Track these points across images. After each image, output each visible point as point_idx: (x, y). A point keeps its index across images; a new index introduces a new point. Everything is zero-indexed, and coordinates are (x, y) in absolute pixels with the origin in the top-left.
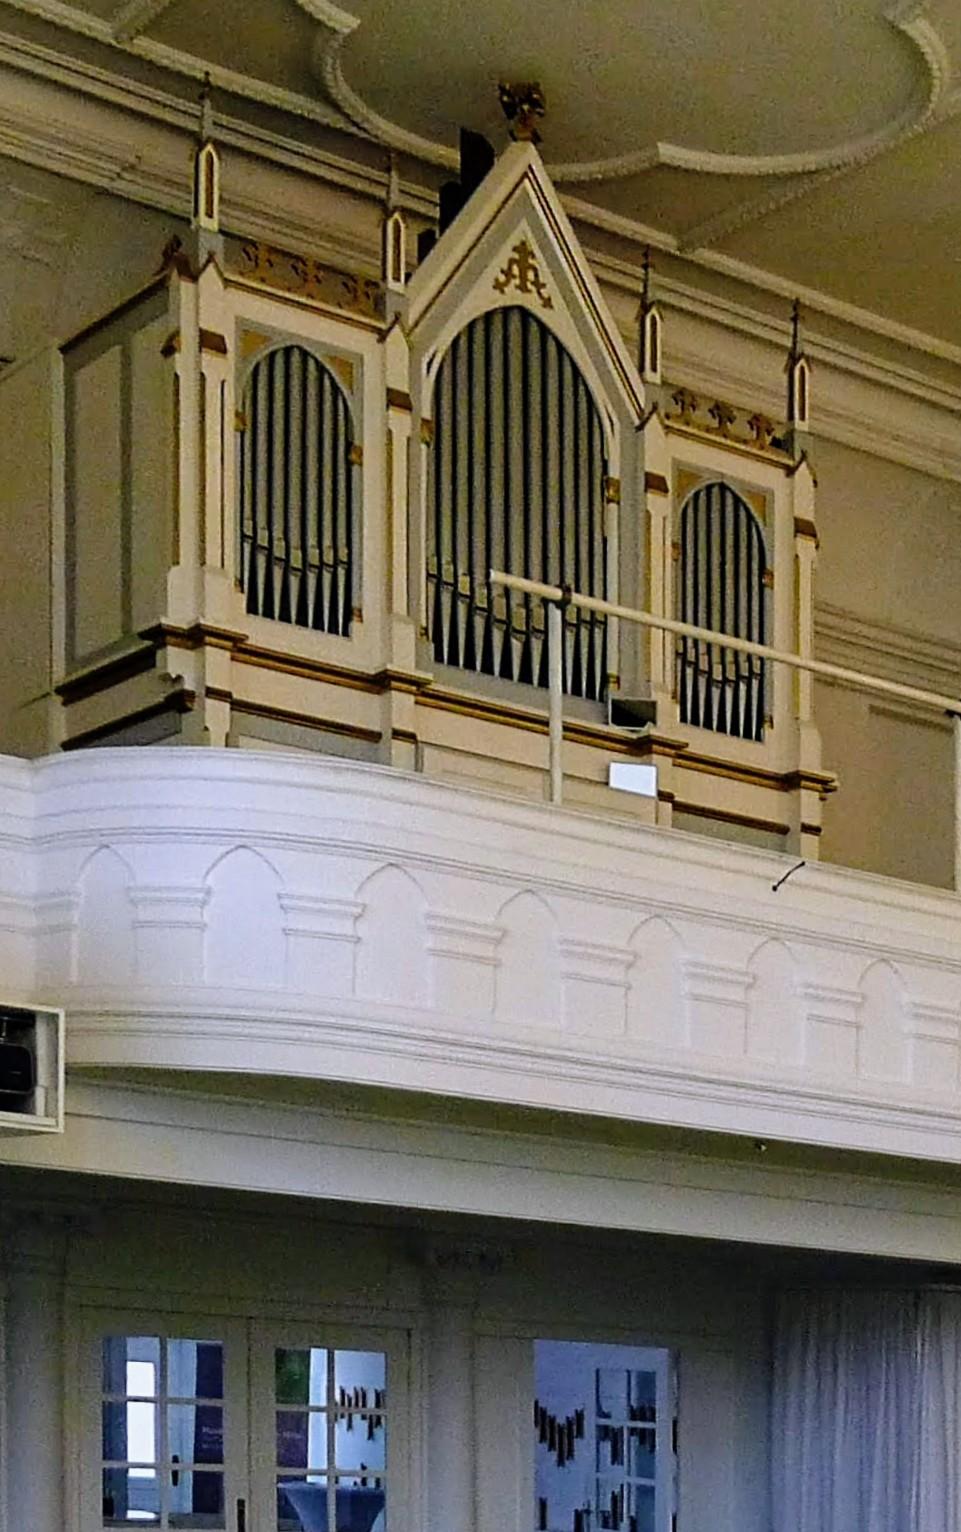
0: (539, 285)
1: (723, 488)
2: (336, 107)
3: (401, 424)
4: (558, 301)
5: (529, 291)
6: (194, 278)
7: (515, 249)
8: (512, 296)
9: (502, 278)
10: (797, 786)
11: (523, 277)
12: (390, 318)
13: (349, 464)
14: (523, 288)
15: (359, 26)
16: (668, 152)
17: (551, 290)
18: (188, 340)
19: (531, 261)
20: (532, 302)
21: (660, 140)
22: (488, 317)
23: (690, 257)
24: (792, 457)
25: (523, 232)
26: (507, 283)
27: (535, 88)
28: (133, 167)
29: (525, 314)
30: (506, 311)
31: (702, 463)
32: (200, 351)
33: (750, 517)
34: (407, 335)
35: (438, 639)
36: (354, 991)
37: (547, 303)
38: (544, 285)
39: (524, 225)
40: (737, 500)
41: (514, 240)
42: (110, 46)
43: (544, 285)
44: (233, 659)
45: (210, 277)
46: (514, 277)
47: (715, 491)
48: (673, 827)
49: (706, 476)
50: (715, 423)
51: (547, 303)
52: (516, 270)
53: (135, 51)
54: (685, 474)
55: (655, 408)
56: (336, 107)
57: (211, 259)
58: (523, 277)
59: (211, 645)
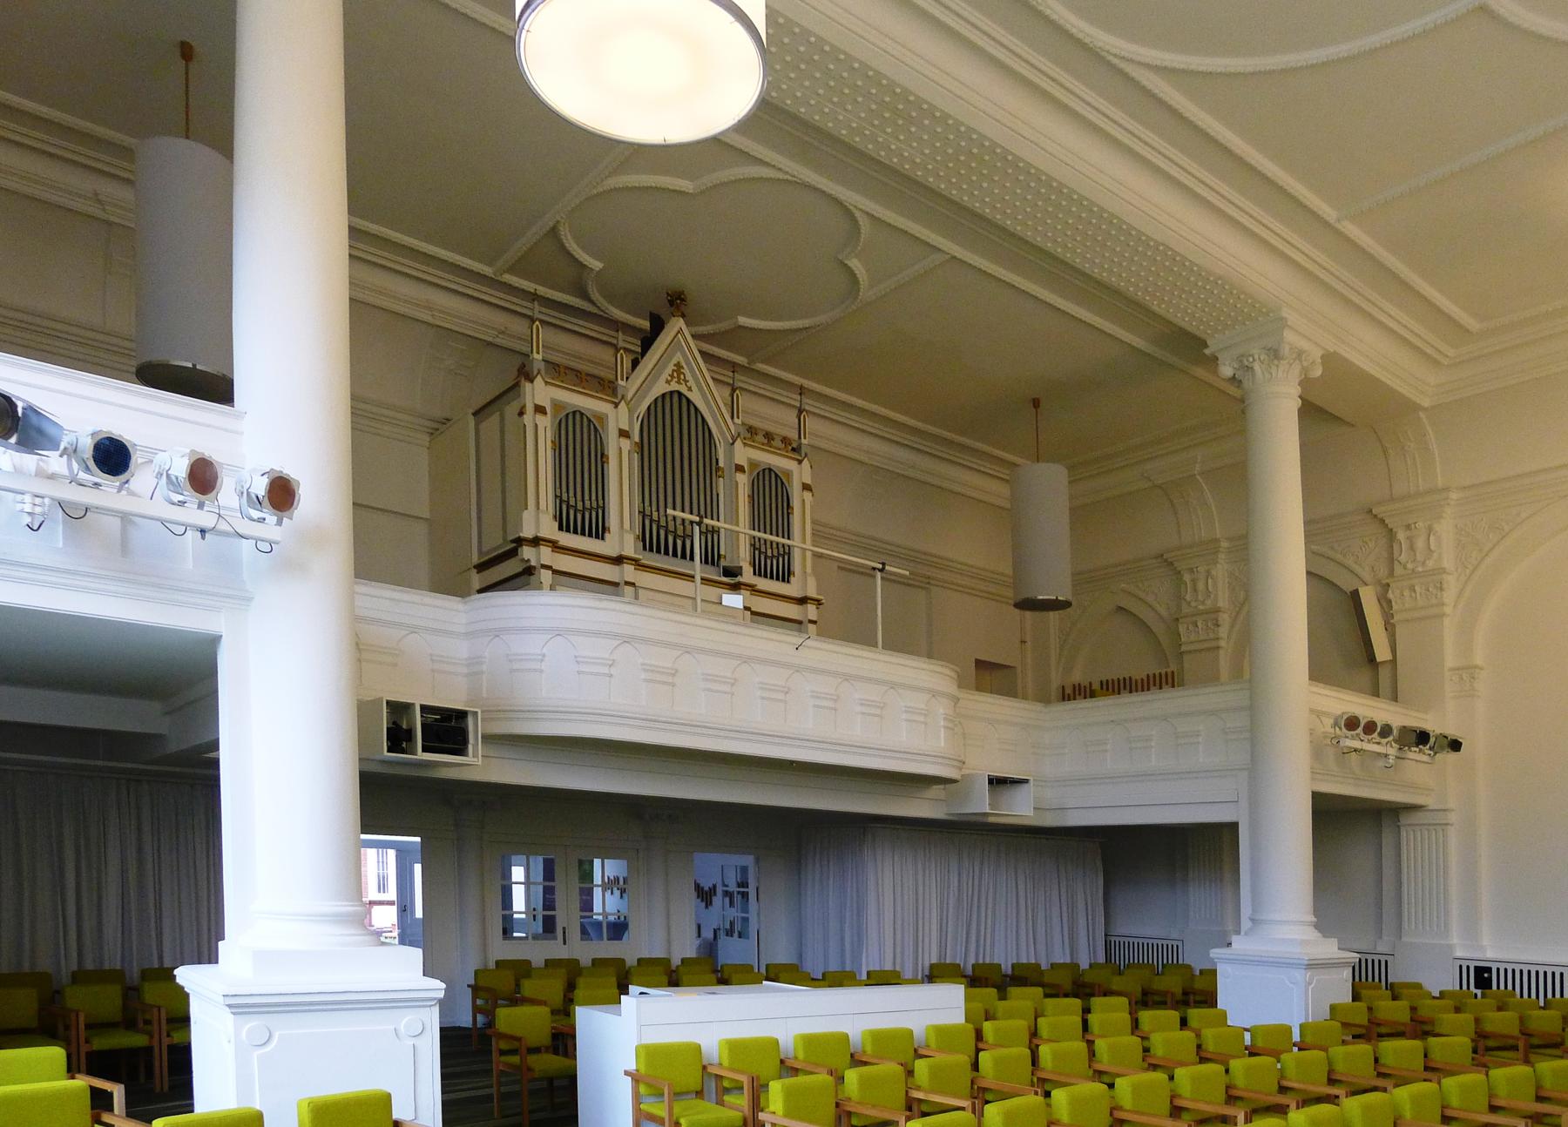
6: (532, 381)
7: (675, 365)
8: (674, 386)
9: (669, 378)
11: (679, 378)
14: (679, 382)
16: (743, 320)
17: (691, 383)
18: (530, 409)
20: (683, 389)
25: (678, 357)
34: (627, 404)
37: (690, 389)
41: (674, 361)
51: (690, 389)
52: (675, 374)
57: (539, 373)
58: (679, 378)
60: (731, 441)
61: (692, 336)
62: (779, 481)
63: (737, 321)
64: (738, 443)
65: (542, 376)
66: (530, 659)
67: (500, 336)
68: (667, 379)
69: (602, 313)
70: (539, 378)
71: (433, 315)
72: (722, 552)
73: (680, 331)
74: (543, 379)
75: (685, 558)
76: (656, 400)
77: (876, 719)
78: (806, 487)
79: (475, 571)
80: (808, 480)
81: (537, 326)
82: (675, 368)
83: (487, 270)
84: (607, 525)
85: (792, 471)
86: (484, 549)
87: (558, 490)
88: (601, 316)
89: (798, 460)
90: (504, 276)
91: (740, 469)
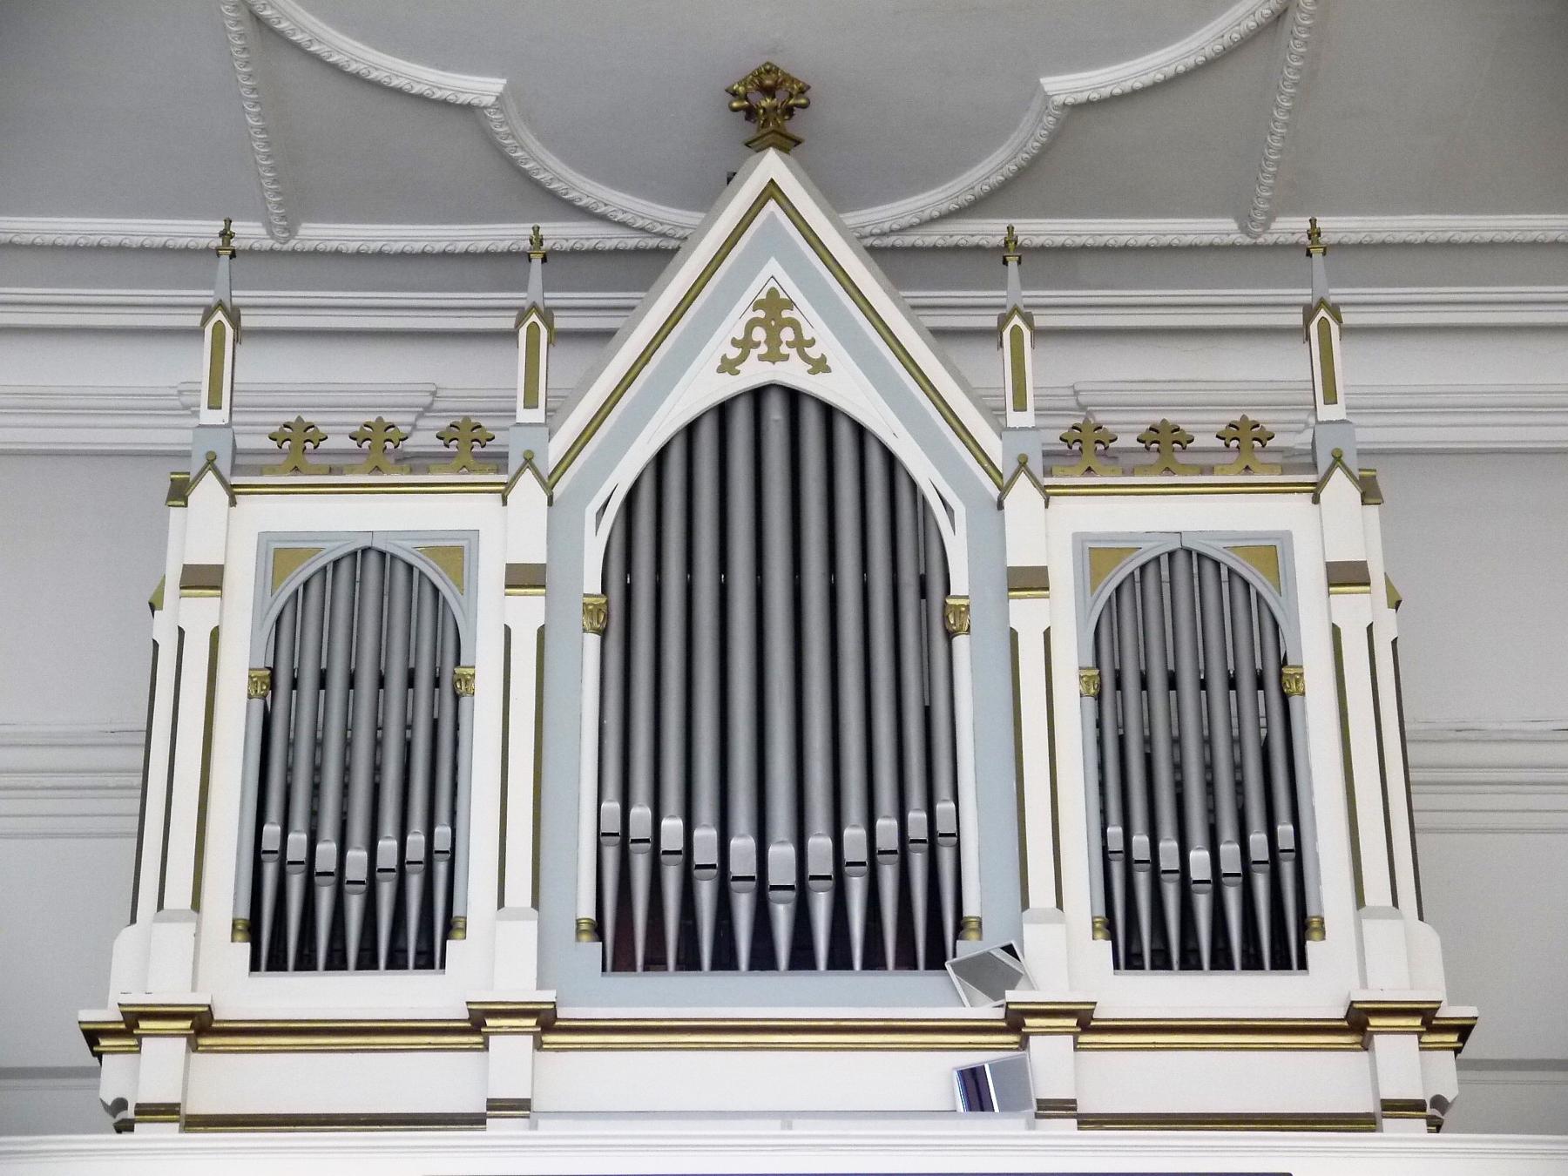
0: (801, 344)
2: (587, 214)
3: (528, 611)
5: (786, 358)
7: (757, 305)
8: (755, 373)
9: (734, 353)
11: (773, 340)
15: (506, 88)
16: (1065, 86)
17: (826, 343)
19: (786, 314)
20: (793, 373)
22: (723, 411)
23: (1269, 239)
25: (773, 275)
27: (770, 70)
28: (428, 408)
29: (794, 398)
30: (758, 395)
31: (1139, 526)
34: (548, 485)
38: (812, 343)
41: (756, 289)
42: (272, 251)
43: (812, 343)
44: (1077, 1047)
46: (757, 345)
48: (127, 1109)
51: (820, 366)
52: (759, 334)
53: (310, 246)
55: (1023, 464)
56: (587, 214)
58: (773, 340)
59: (119, 1022)
60: (995, 493)
62: (1239, 588)
63: (1047, 97)
64: (1023, 493)
65: (1031, 475)
68: (724, 358)
73: (772, 191)
74: (1036, 483)
75: (848, 965)
76: (691, 430)
81: (1016, 330)
82: (761, 314)
83: (1221, 229)
84: (1312, 911)
85: (264, 538)
87: (1115, 831)
90: (1274, 226)
91: (1031, 581)
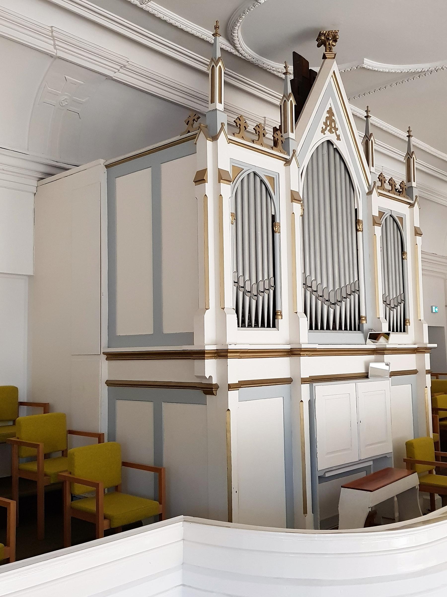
1: (255, 174)
4: (342, 137)
6: (215, 138)
10: (226, 357)
12: (291, 154)
13: (273, 232)
14: (331, 131)
18: (211, 176)
21: (365, 58)
24: (289, 154)
25: (330, 103)
26: (326, 128)
32: (219, 182)
33: (267, 189)
35: (237, 312)
36: (392, 452)
37: (338, 138)
39: (330, 101)
40: (262, 181)
45: (222, 138)
47: (252, 175)
49: (245, 169)
50: (256, 138)
51: (338, 138)
54: (237, 170)
57: (222, 128)
58: (331, 124)
61: (224, 73)
66: (44, 173)
67: (121, 70)
69: (240, 56)
70: (222, 135)
71: (55, 45)
72: (363, 314)
77: (54, 106)
78: (417, 232)
79: (105, 357)
80: (417, 225)
86: (121, 331)
88: (236, 55)
89: (409, 203)
